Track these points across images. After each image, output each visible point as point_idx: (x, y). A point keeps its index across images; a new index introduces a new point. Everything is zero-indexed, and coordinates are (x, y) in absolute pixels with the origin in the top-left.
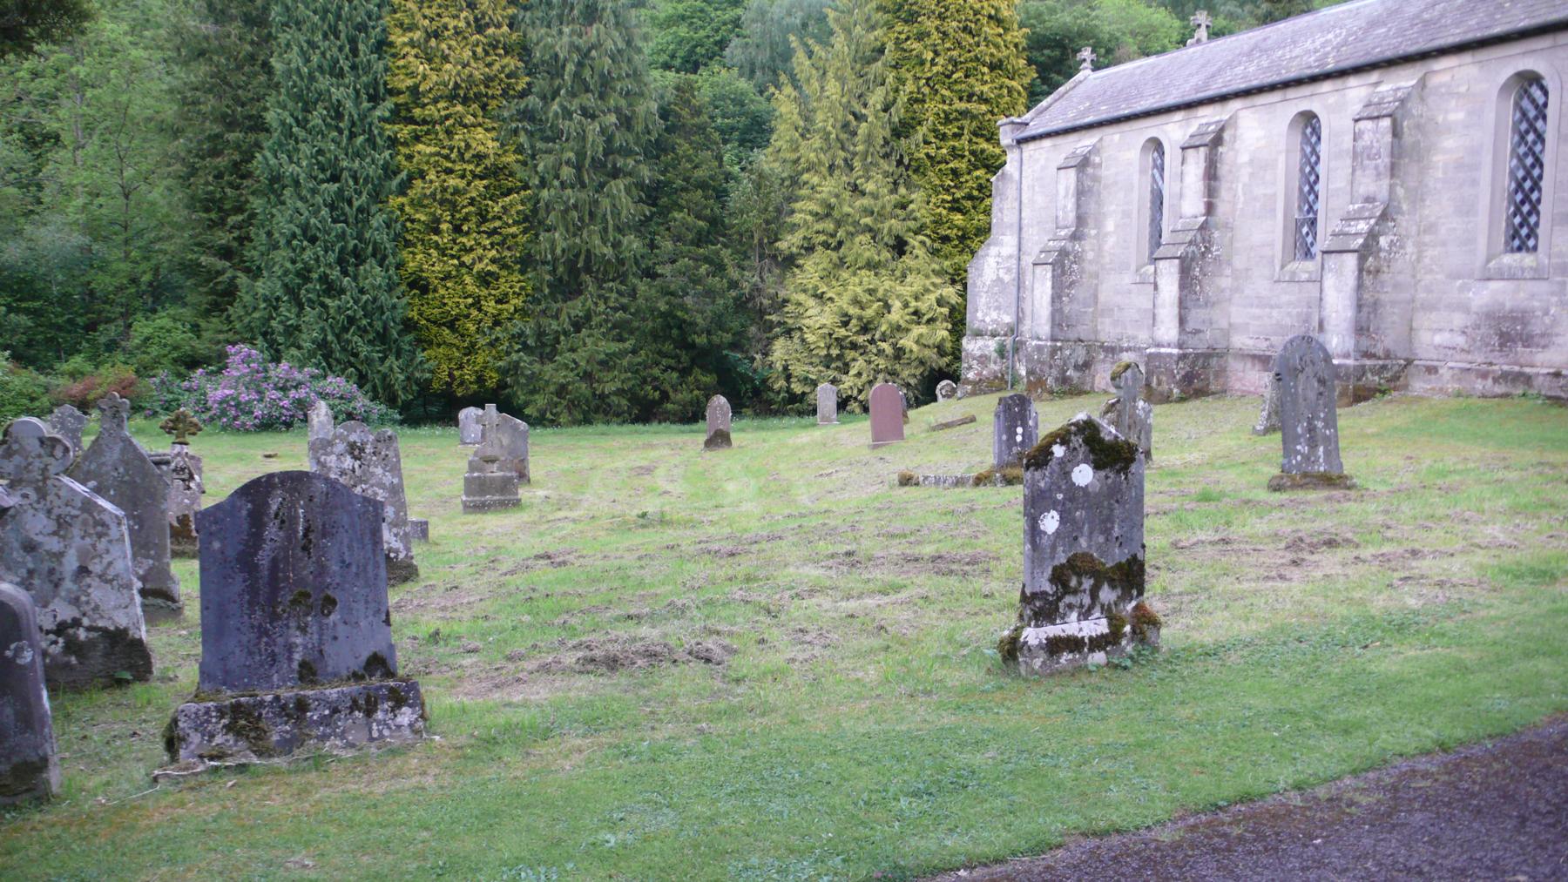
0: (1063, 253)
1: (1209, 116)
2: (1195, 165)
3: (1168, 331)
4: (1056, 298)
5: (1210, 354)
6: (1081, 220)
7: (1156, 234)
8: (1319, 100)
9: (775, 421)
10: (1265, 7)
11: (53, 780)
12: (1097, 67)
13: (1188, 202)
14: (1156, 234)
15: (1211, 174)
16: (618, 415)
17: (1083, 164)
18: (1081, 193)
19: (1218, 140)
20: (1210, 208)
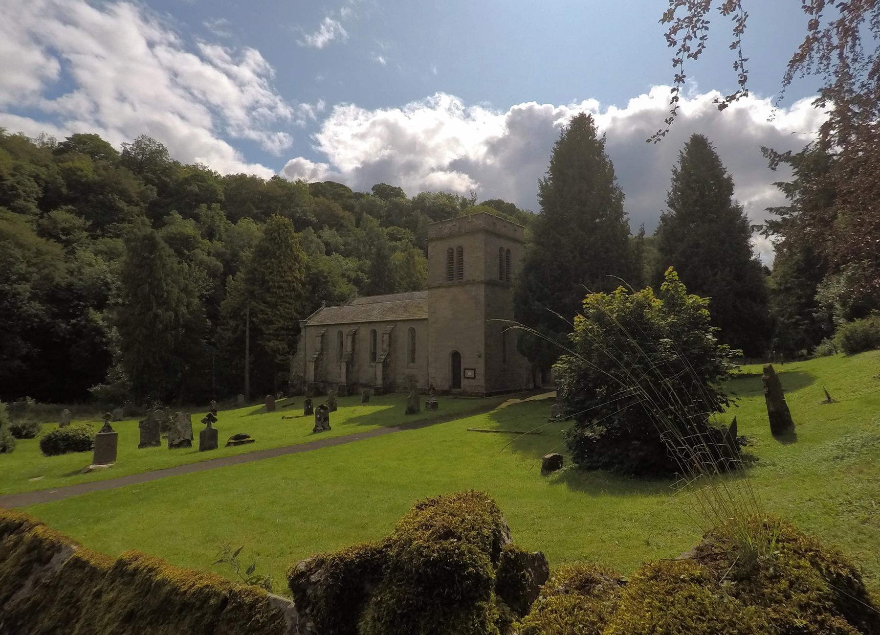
0: (317, 358)
1: (355, 328)
2: (350, 339)
3: (343, 379)
4: (315, 370)
5: (355, 384)
6: (322, 350)
7: (341, 355)
8: (376, 327)
9: (642, 491)
10: (740, 352)
11: (760, 103)
12: (327, 306)
13: (348, 347)
14: (341, 355)
15: (353, 341)
16: (398, 567)
17: (323, 336)
18: (322, 342)
19: (355, 334)
20: (353, 350)
